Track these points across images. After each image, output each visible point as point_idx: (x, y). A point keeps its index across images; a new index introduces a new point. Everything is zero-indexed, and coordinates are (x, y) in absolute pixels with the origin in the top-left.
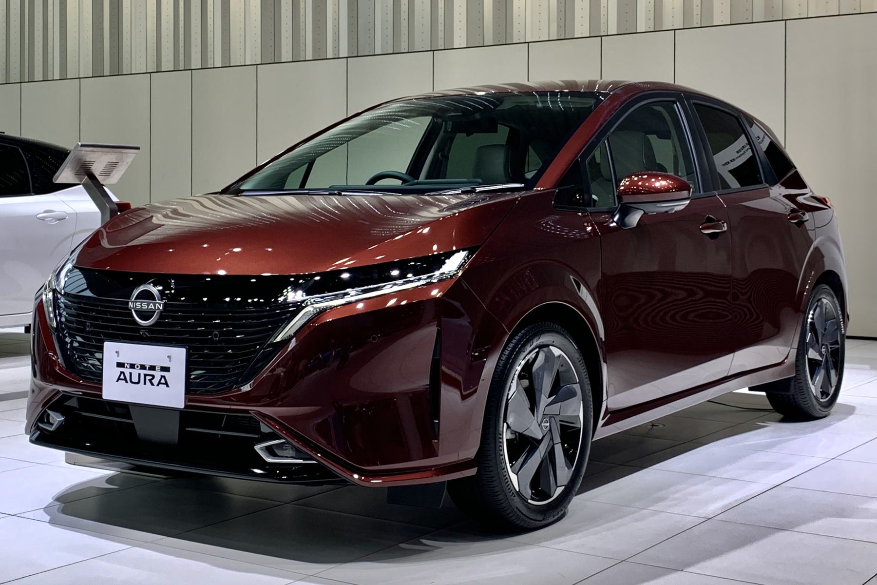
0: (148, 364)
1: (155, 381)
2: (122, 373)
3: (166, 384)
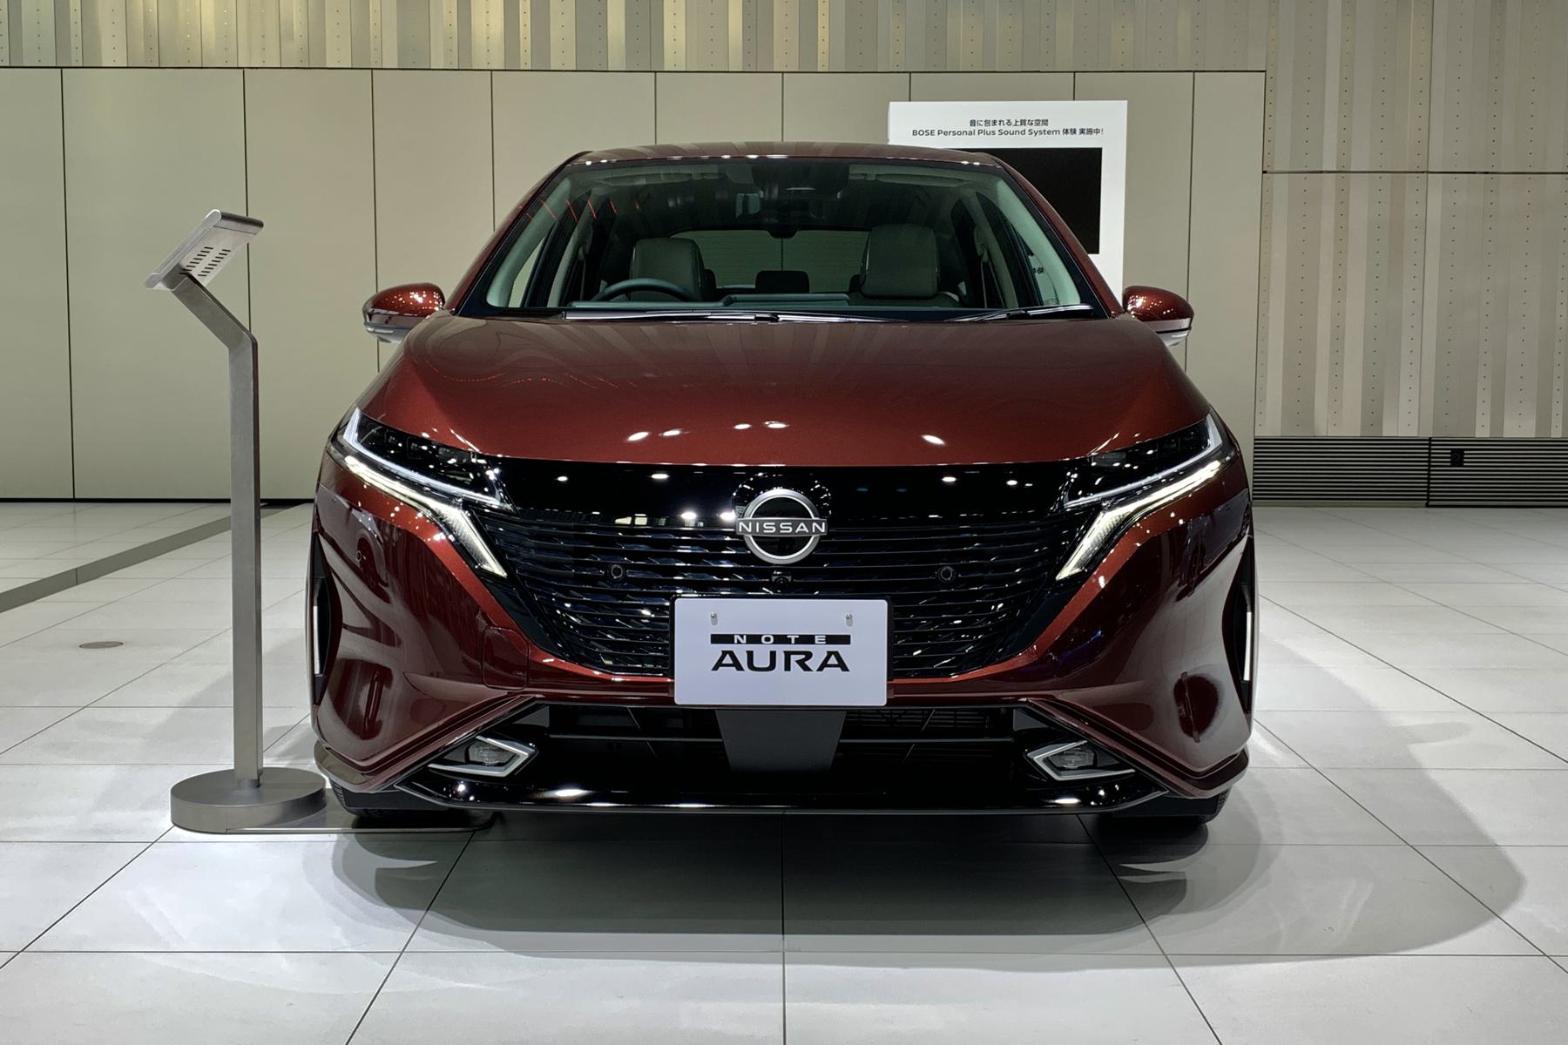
0: (793, 632)
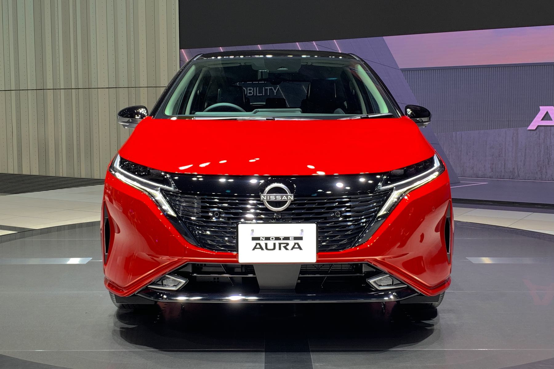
1: (289, 247)
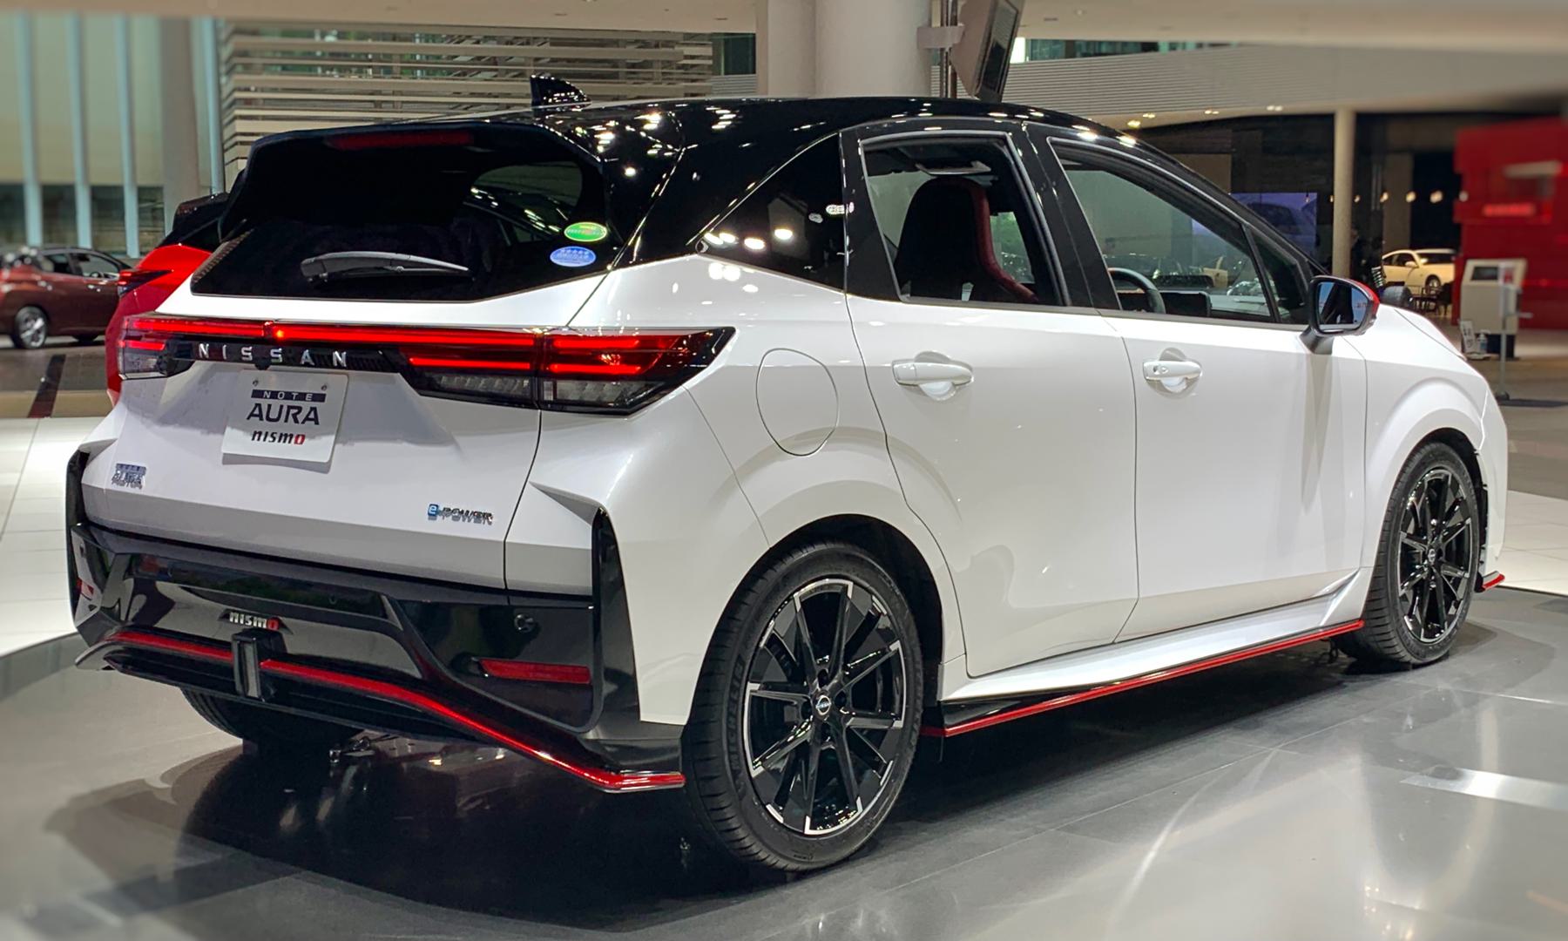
1: (301, 417)
2: (258, 405)
3: (316, 421)
